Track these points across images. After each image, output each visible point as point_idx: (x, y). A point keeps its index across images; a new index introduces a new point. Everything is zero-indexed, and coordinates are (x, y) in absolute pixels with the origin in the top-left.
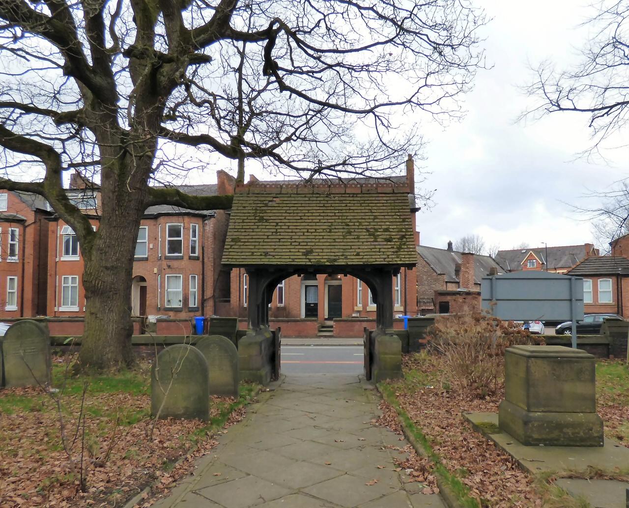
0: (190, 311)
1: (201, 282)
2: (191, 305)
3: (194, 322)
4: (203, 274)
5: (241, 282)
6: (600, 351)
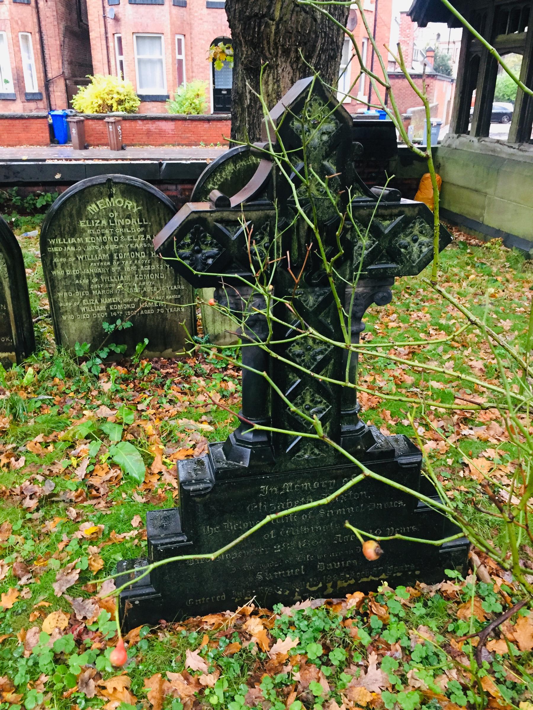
0: (28, 100)
1: (39, 47)
4: (40, 32)
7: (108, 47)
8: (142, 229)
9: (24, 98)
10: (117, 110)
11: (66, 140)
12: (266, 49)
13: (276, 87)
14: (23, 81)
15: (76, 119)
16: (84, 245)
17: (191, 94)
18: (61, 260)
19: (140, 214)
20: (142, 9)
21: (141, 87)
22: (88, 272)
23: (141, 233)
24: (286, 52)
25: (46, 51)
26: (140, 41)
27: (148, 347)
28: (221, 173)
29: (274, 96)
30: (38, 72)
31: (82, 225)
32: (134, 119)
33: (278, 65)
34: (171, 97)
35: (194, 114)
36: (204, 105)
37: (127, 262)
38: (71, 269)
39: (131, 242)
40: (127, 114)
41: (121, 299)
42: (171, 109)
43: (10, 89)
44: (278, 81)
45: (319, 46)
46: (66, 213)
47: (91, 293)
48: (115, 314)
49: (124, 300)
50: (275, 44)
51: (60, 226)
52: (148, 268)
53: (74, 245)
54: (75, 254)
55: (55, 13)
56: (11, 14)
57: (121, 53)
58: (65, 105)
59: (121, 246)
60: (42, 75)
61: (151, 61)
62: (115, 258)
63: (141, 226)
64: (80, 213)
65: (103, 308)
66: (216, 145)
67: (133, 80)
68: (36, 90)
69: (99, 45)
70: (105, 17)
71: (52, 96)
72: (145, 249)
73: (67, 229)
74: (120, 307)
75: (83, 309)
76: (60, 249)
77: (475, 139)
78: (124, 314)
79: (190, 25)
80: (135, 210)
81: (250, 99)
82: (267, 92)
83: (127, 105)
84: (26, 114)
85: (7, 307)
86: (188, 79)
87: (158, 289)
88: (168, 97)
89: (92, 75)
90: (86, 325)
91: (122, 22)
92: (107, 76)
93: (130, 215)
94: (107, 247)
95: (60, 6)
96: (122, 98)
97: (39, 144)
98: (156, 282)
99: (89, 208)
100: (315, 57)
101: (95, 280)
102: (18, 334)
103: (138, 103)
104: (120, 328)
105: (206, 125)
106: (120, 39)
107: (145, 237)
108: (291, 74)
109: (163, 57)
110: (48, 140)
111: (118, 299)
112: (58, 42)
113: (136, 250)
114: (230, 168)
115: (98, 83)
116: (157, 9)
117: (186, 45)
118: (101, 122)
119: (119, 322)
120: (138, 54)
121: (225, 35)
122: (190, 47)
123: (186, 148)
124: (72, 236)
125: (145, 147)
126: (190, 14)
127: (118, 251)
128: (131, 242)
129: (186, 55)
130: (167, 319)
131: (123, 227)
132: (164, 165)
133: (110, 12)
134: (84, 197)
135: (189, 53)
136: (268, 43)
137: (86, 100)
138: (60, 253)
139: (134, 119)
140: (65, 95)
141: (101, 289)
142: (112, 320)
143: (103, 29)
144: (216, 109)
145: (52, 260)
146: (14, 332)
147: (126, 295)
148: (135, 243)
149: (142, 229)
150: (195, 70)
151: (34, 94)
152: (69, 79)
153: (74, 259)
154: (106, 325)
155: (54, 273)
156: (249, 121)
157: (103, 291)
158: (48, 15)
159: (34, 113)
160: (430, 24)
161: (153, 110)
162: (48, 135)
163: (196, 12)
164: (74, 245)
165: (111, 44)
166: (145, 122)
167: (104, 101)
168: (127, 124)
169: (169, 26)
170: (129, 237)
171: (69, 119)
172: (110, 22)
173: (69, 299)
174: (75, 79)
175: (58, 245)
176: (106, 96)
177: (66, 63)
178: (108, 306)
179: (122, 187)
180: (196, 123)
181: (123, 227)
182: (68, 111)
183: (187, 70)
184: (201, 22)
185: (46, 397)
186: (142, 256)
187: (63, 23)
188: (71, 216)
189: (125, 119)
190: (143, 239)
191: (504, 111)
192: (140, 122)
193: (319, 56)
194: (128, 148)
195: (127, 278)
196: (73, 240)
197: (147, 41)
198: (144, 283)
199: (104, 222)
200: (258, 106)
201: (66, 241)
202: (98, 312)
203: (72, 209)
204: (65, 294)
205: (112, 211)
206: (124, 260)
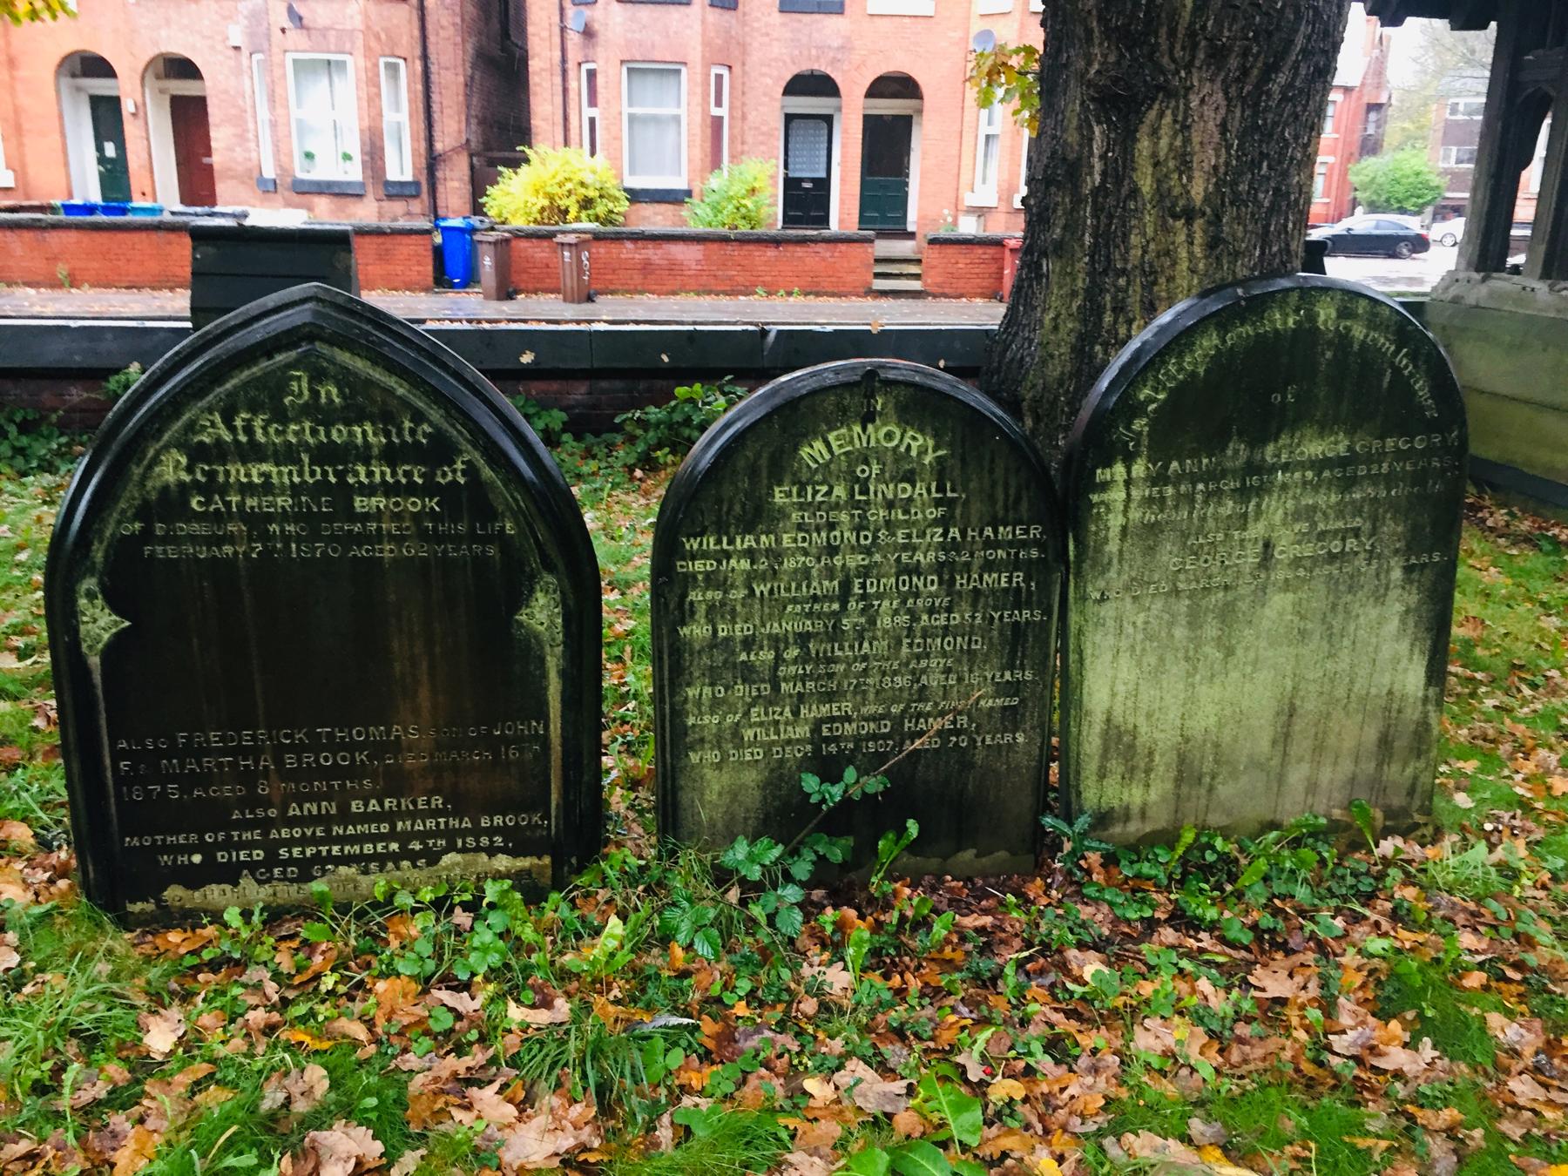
0: (390, 197)
1: (419, 87)
2: (393, 174)
3: (438, 239)
4: (425, 57)
5: (572, 95)
6: (1278, 316)
7: (565, 91)
8: (940, 511)
9: (381, 193)
10: (578, 219)
11: (469, 279)
12: (1164, 47)
13: (1178, 143)
14: (382, 159)
15: (493, 236)
16: (776, 555)
17: (738, 189)
18: (709, 595)
19: (941, 471)
20: (645, 12)
21: (632, 172)
22: (776, 629)
23: (936, 522)
24: (1217, 55)
25: (435, 97)
26: (637, 79)
27: (914, 847)
28: (1180, 356)
29: (1171, 164)
30: (414, 138)
31: (779, 498)
32: (618, 238)
33: (1189, 89)
34: (696, 193)
35: (744, 228)
36: (765, 211)
37: (886, 603)
38: (734, 622)
39: (905, 548)
40: (602, 228)
41: (856, 708)
42: (696, 218)
43: (353, 173)
44: (1185, 128)
45: (1300, 41)
46: (741, 464)
47: (776, 688)
48: (833, 748)
49: (864, 710)
50: (1191, 34)
51: (720, 501)
52: (942, 620)
53: (750, 554)
54: (750, 578)
55: (458, 20)
56: (366, 16)
57: (593, 102)
58: (467, 208)
59: (877, 557)
60: (423, 145)
61: (656, 119)
62: (857, 590)
63: (938, 503)
64: (780, 465)
65: (803, 731)
66: (790, 294)
67: (615, 160)
68: (408, 176)
69: (546, 84)
70: (563, 29)
71: (440, 189)
72: (939, 568)
73: (737, 508)
74: (849, 729)
75: (748, 734)
76: (710, 565)
77: (1542, 287)
78: (857, 748)
79: (744, 48)
80: (927, 460)
81: (1104, 174)
82: (1154, 155)
83: (600, 209)
84: (386, 224)
85: (546, 728)
86: (733, 157)
87: (960, 680)
88: (689, 193)
89: (530, 147)
90: (751, 777)
91: (601, 38)
92: (561, 149)
93: (912, 471)
94: (838, 561)
95: (470, 8)
96: (592, 193)
97: (410, 287)
98: (959, 661)
99: (805, 452)
100: (1286, 69)
101: (793, 652)
102: (567, 806)
103: (624, 206)
104: (856, 793)
105: (771, 252)
106: (592, 74)
107: (945, 534)
108: (1223, 111)
109: (683, 111)
110: (430, 279)
111: (847, 706)
112: (461, 79)
113: (916, 570)
114: (1209, 342)
115: (543, 162)
116: (674, 13)
117: (732, 87)
118: (545, 244)
119: (850, 774)
120: (630, 105)
121: (816, 67)
122: (740, 92)
123: (724, 300)
124: (749, 528)
125: (637, 297)
126: (744, 24)
127: (865, 572)
128: (905, 548)
129: (731, 108)
130: (972, 765)
131: (890, 505)
132: (772, 336)
133: (576, 18)
134: (794, 420)
135: (738, 104)
136: (1172, 33)
137: (515, 198)
138: (707, 575)
139: (618, 238)
140: (469, 187)
141: (803, 679)
142: (829, 770)
143: (557, 54)
144: (788, 220)
145: (684, 595)
146: (554, 797)
147: (871, 696)
148: (914, 549)
149: (940, 511)
150: (749, 139)
151: (402, 184)
152: (478, 154)
153: (742, 593)
154: (810, 783)
155: (684, 631)
156: (1096, 228)
157: (810, 685)
158: (444, 22)
159: (402, 223)
160: (1411, 22)
161: (656, 219)
162: (430, 268)
163: (758, 20)
164: (750, 554)
165: (573, 85)
166: (640, 244)
167: (551, 198)
168: (602, 249)
169: (699, 48)
170: (900, 533)
171: (477, 237)
172: (574, 39)
173: (716, 703)
174: (489, 154)
175: (705, 555)
176: (555, 190)
177: (474, 121)
178: (816, 729)
179: (903, 392)
180: (751, 247)
181: (890, 505)
182: (475, 221)
183: (732, 139)
184: (766, 39)
185: (675, 1021)
186: (931, 585)
187: (473, 40)
188: (753, 472)
189: (598, 237)
190: (937, 539)
191: (1401, 233)
192: (629, 245)
193: (1295, 68)
194: (600, 299)
195: (882, 645)
196: (749, 541)
197: (651, 80)
198: (923, 663)
199: (840, 491)
200: (1124, 191)
201: (731, 542)
202: (789, 742)
203: (758, 456)
204: (707, 690)
205: (867, 463)
206: (880, 596)
